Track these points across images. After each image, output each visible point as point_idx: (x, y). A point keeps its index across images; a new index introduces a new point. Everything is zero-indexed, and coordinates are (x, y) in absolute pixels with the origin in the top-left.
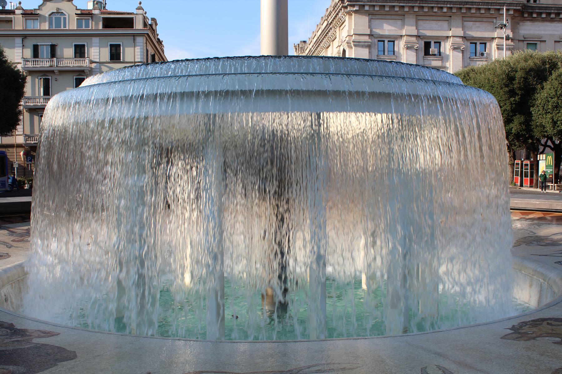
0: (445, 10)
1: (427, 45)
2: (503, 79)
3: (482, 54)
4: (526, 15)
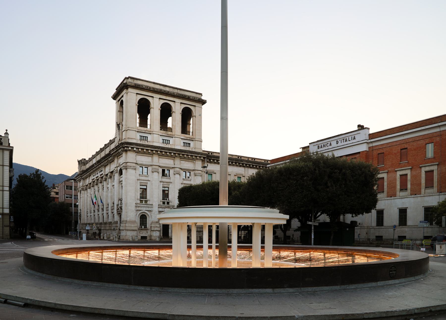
0: (172, 154)
1: (163, 171)
3: (189, 178)
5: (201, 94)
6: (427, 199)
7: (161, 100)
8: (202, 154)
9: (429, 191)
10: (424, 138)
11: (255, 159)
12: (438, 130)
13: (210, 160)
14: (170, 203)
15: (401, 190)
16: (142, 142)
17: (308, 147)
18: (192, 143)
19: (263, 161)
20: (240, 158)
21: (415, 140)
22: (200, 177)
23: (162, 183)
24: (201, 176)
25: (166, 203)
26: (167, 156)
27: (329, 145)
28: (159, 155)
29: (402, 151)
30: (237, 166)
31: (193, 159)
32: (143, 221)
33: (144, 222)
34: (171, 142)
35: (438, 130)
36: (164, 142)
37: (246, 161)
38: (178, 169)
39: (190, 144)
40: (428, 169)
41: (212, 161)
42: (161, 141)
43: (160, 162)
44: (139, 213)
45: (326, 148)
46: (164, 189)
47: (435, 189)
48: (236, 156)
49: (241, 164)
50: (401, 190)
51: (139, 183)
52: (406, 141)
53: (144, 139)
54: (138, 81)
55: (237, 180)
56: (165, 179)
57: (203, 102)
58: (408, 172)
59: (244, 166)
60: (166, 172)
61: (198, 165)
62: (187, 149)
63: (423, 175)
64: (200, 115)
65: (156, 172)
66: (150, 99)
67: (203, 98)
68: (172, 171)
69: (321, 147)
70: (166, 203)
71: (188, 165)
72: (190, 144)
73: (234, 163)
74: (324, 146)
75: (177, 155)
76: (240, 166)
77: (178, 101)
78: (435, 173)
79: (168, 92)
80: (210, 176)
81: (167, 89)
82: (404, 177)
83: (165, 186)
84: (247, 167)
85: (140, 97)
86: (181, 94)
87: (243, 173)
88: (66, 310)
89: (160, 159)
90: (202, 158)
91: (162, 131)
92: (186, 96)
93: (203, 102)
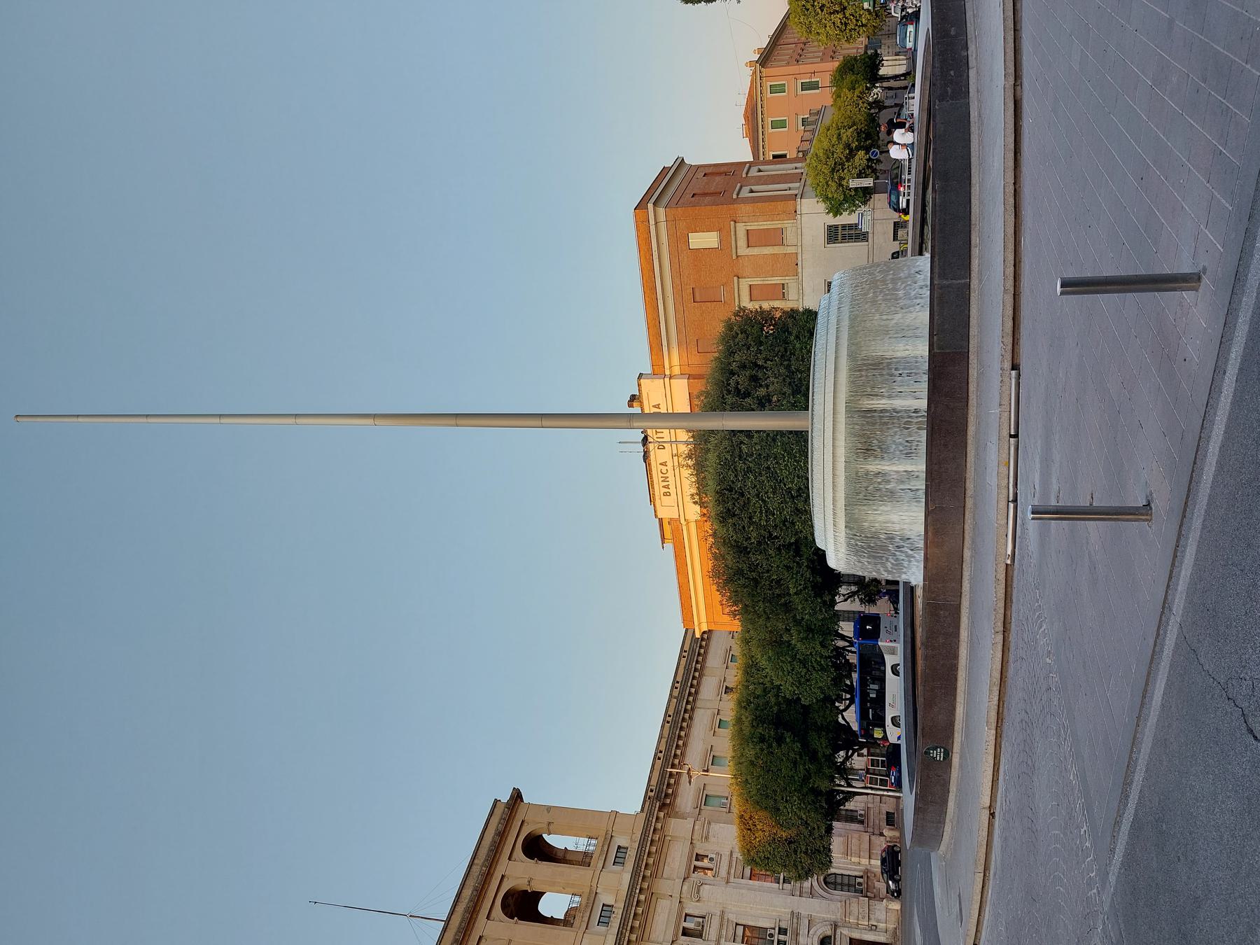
0: (642, 897)
1: (686, 932)
2: (762, 750)
3: (711, 859)
4: (668, 801)
5: (496, 801)
6: (807, 239)
7: (493, 914)
8: (650, 813)
9: (790, 236)
10: (675, 253)
11: (675, 681)
12: (663, 226)
13: (667, 795)
14: (783, 925)
15: (784, 297)
16: (630, 865)
17: (661, 521)
18: (621, 840)
19: (684, 661)
20: (669, 719)
21: (677, 272)
22: (713, 825)
23: (732, 879)
24: (709, 823)
25: (782, 937)
26: (646, 913)
27: (664, 468)
28: (655, 875)
29: (698, 299)
30: (689, 726)
31: (663, 840)
32: (842, 884)
33: (846, 881)
34: (609, 900)
35: (663, 226)
36: (606, 920)
37: (679, 702)
38: (685, 888)
39: (619, 847)
40: (742, 242)
41: (670, 791)
42: (602, 929)
43: (661, 939)
44: (821, 891)
45: (670, 474)
46: (739, 939)
47: (787, 224)
48: (663, 726)
49: (687, 716)
50: (784, 297)
51: (737, 880)
52: (678, 290)
53: (607, 914)
54: (463, 895)
55: (734, 696)
56: (712, 931)
57: (517, 796)
58: (745, 284)
59: (692, 709)
60: (690, 925)
61: (679, 829)
62: (631, 855)
63: (755, 251)
64: (549, 809)
65: (698, 892)
66: (506, 887)
67: (505, 798)
68: (691, 908)
69: (667, 487)
70: (782, 937)
71: (676, 859)
72: (619, 847)
73: (683, 733)
74: (665, 479)
75: (645, 885)
76: (691, 718)
77: (503, 867)
78: (753, 226)
79: (475, 889)
80: (711, 801)
81: (468, 893)
82: (755, 292)
83: (731, 932)
84: (694, 700)
85: (519, 851)
86: (488, 855)
87: (709, 712)
88: (1014, 319)
89: (653, 937)
90: (662, 814)
91: (577, 923)
92: (494, 841)
93: (517, 796)
